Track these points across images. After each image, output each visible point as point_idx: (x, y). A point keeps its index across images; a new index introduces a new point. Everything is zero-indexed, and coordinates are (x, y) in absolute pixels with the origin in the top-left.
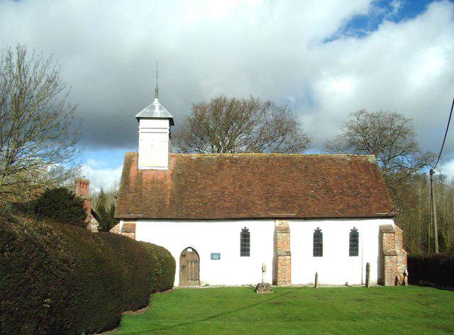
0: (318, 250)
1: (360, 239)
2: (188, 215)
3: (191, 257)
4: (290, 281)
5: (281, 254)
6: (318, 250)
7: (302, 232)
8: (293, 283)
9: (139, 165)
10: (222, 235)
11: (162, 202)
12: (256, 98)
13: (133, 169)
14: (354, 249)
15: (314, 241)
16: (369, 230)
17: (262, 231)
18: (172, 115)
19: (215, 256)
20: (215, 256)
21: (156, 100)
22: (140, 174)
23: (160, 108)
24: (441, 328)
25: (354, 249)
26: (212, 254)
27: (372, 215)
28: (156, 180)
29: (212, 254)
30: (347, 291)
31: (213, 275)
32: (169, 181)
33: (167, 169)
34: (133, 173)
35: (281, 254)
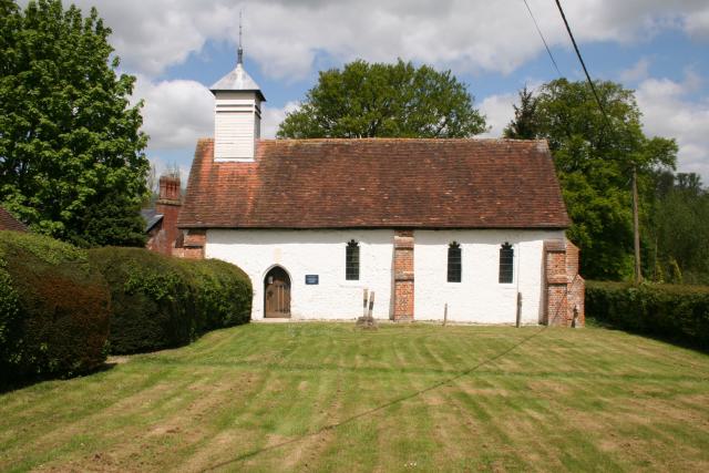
0: (454, 273)
1: (515, 260)
2: (488, 220)
3: (278, 276)
4: (412, 315)
5: (403, 280)
6: (454, 273)
7: (430, 255)
8: (416, 318)
9: (215, 156)
10: (325, 255)
11: (241, 205)
12: (406, 62)
13: (206, 162)
14: (506, 274)
15: (449, 260)
16: (529, 252)
17: (377, 254)
18: (259, 84)
19: (312, 280)
20: (312, 280)
21: (239, 65)
22: (216, 167)
23: (244, 77)
24: (303, 367)
25: (506, 274)
26: (307, 277)
27: (534, 225)
28: (237, 175)
29: (307, 277)
30: (338, 328)
31: (306, 305)
32: (254, 177)
33: (252, 160)
34: (206, 167)
35: (403, 280)
